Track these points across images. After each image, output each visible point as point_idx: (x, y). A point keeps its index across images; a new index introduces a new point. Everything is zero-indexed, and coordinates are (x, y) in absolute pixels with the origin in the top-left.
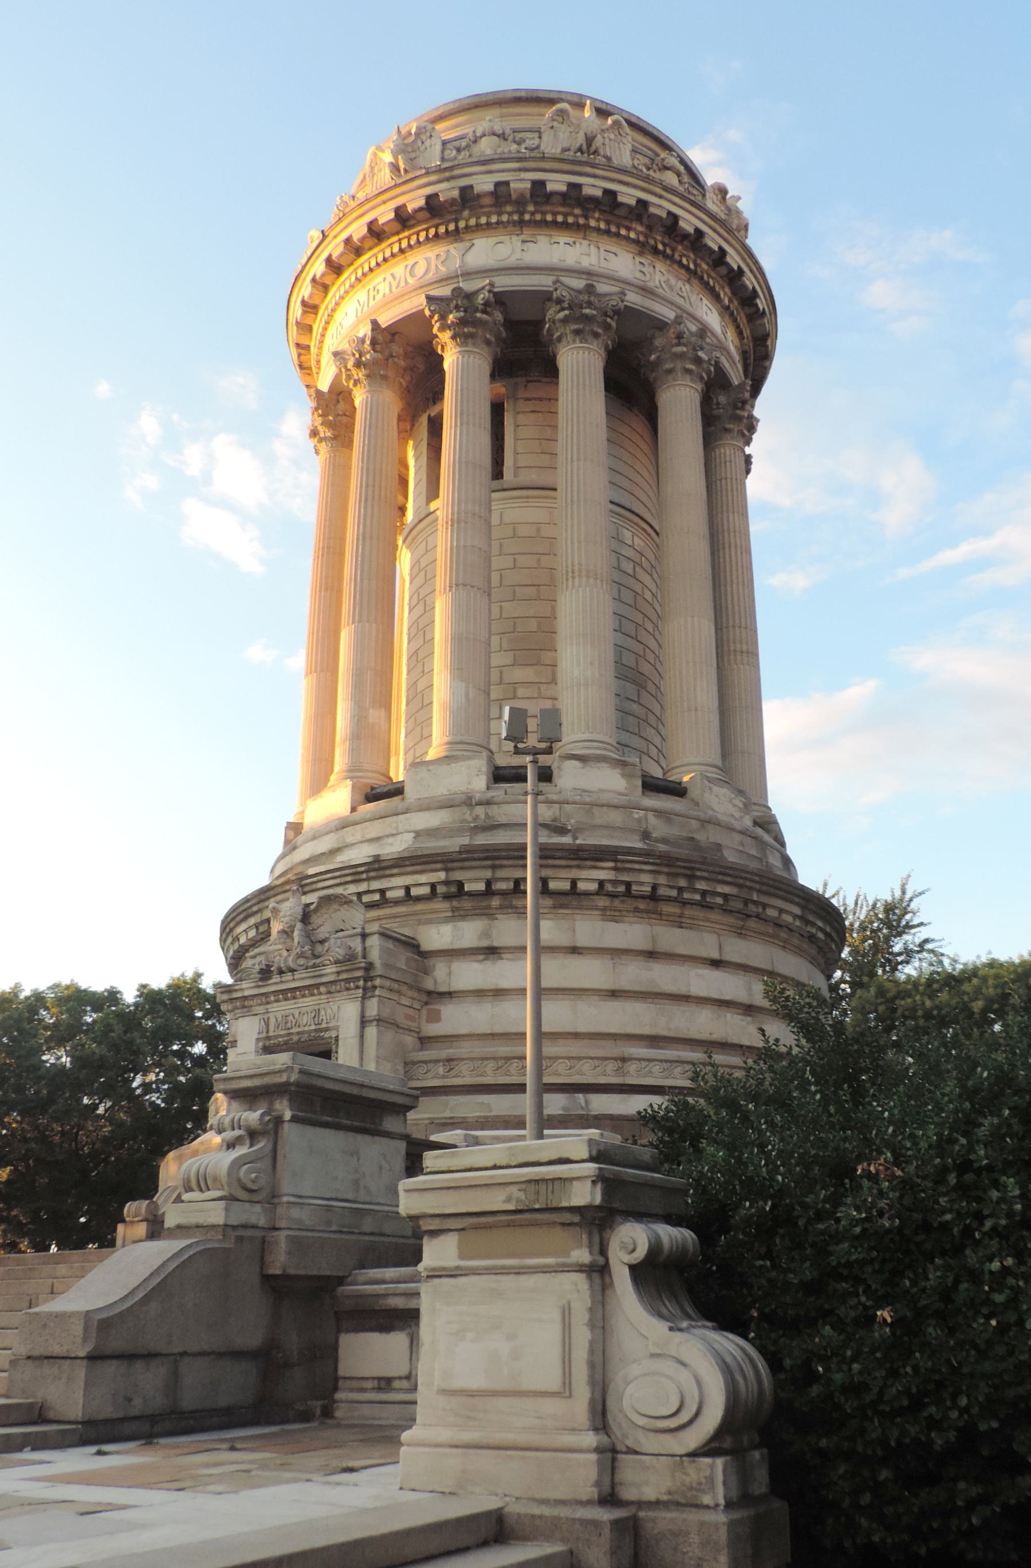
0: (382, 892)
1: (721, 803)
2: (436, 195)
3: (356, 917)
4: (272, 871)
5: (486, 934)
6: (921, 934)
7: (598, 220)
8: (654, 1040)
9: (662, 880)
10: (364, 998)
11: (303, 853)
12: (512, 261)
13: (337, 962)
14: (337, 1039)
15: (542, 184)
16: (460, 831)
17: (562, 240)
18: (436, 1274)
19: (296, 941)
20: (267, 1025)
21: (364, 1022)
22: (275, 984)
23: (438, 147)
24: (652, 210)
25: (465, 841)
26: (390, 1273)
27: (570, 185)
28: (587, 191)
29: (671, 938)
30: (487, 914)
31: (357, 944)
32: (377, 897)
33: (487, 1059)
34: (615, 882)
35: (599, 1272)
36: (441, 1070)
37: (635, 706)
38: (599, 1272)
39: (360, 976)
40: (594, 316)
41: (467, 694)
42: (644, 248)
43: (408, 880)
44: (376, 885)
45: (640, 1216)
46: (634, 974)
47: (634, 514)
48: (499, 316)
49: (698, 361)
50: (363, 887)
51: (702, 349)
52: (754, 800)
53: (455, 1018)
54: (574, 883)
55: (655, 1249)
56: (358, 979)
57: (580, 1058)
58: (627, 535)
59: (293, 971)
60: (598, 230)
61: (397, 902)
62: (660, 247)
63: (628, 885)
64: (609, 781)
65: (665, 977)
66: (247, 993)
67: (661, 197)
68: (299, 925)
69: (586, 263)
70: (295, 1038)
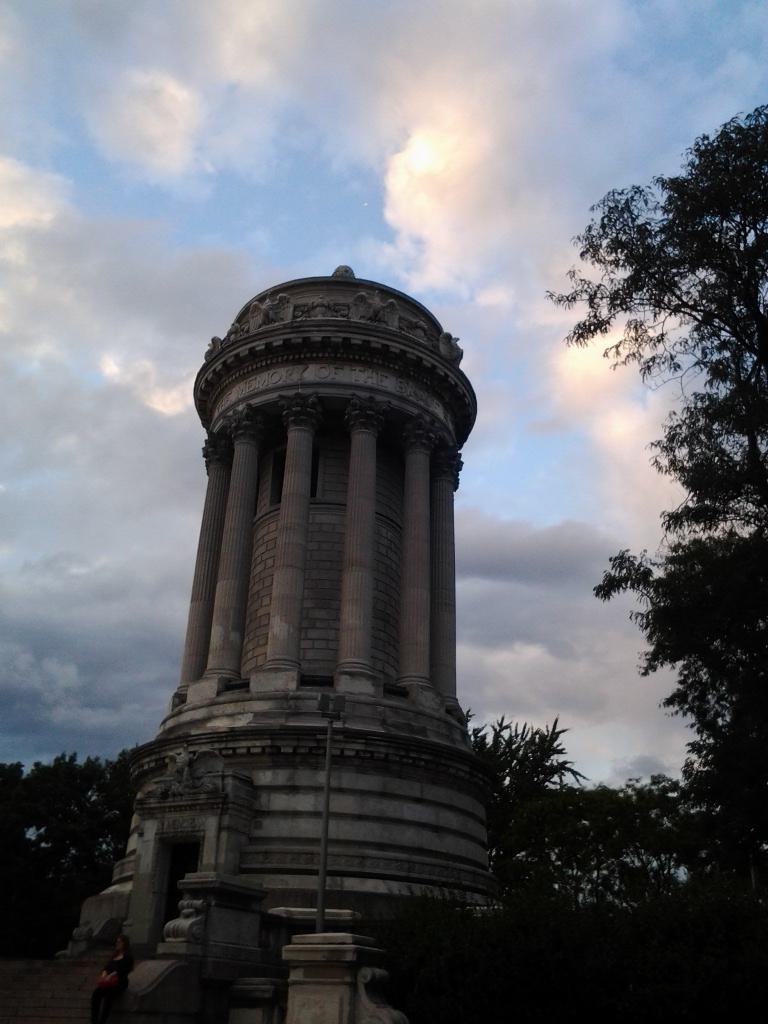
0: (234, 749)
1: (427, 701)
2: (290, 339)
3: (219, 765)
4: (164, 722)
5: (291, 778)
6: (561, 758)
7: (378, 359)
8: (380, 846)
9: (391, 751)
10: (221, 814)
11: (186, 717)
12: (329, 380)
13: (207, 793)
14: (204, 837)
15: (348, 339)
16: (280, 715)
17: (358, 369)
18: (295, 983)
19: (185, 777)
20: (163, 825)
21: (220, 829)
22: (170, 802)
23: (292, 309)
24: (409, 355)
25: (282, 721)
26: (257, 980)
27: (364, 341)
28: (373, 345)
29: (396, 785)
30: (294, 766)
31: (219, 782)
32: (231, 752)
33: (287, 853)
34: (365, 752)
35: (354, 986)
36: (261, 858)
37: (382, 634)
38: (354, 986)
39: (218, 802)
40: (372, 416)
41: (289, 631)
42: (402, 374)
43: (249, 744)
44: (231, 745)
45: (370, 965)
46: (373, 806)
47: (391, 519)
48: (319, 409)
49: (430, 439)
50: (223, 746)
51: (432, 431)
52: (446, 694)
53: (273, 828)
54: (342, 751)
55: (374, 977)
56: (217, 804)
57: (339, 856)
58: (384, 531)
59: (181, 795)
60: (378, 364)
61: (242, 755)
62: (412, 373)
63: (372, 753)
64: (363, 688)
65: (390, 808)
66: (152, 806)
67: (414, 348)
68: (186, 769)
69: (370, 382)
70: (180, 835)
